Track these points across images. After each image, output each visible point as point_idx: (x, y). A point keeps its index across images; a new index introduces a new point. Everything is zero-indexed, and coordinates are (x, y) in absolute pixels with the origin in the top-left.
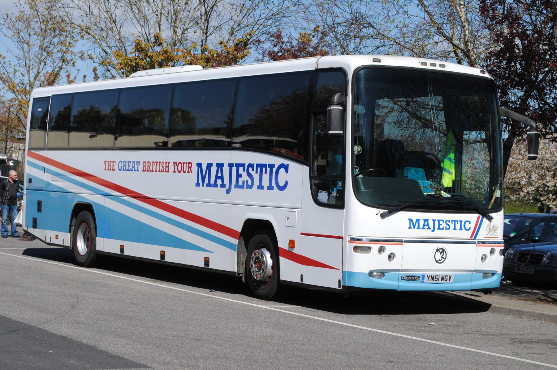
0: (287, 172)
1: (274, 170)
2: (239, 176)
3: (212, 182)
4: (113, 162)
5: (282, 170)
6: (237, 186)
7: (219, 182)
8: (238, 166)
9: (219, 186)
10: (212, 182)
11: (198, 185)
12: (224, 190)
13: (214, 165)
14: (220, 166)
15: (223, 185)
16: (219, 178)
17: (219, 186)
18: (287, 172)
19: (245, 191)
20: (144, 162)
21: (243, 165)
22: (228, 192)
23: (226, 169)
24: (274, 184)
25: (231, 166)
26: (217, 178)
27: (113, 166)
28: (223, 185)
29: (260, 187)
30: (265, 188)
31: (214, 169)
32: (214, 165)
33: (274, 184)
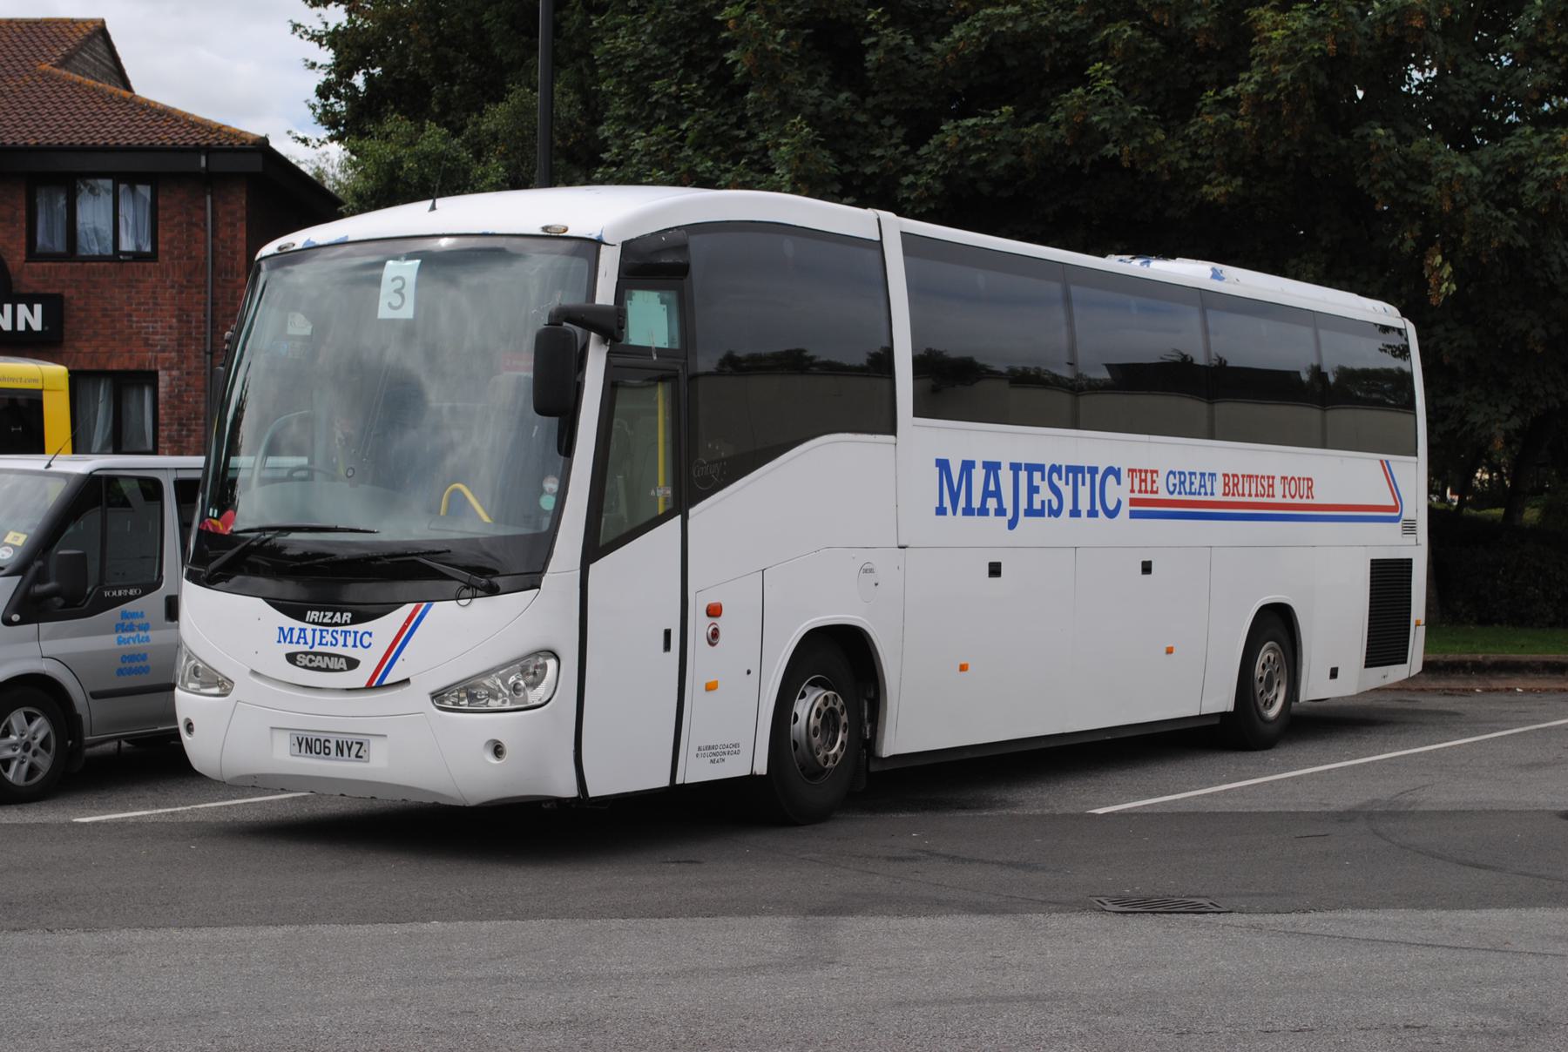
0: (1119, 483)
1: (1098, 478)
2: (1032, 490)
3: (976, 504)
4: (1153, 472)
5: (1111, 479)
6: (1030, 512)
7: (992, 504)
8: (1031, 468)
9: (992, 512)
10: (976, 504)
11: (941, 511)
12: (1003, 521)
13: (979, 465)
14: (992, 468)
15: (1000, 511)
16: (992, 494)
17: (992, 512)
18: (1119, 483)
19: (1047, 521)
20: (1225, 475)
21: (1040, 468)
22: (1012, 524)
23: (1006, 476)
24: (1098, 507)
25: (1015, 468)
26: (987, 494)
27: (1153, 482)
28: (1000, 511)
29: (1075, 513)
30: (1084, 514)
31: (978, 475)
32: (979, 465)
33: (1098, 507)
